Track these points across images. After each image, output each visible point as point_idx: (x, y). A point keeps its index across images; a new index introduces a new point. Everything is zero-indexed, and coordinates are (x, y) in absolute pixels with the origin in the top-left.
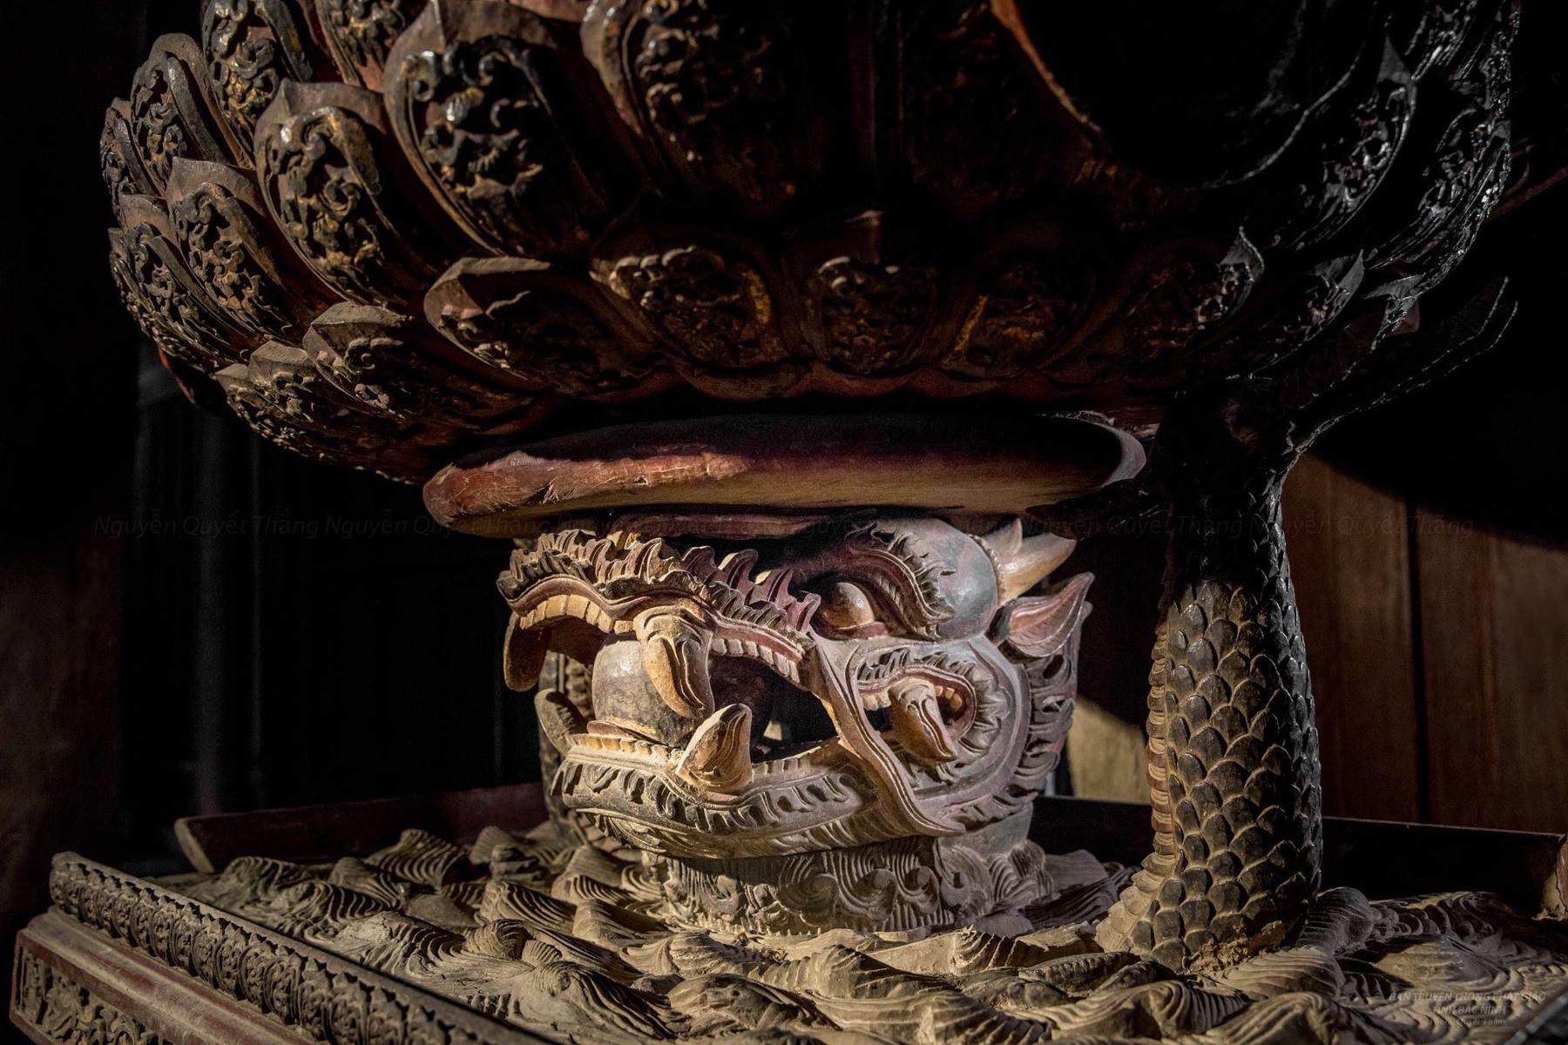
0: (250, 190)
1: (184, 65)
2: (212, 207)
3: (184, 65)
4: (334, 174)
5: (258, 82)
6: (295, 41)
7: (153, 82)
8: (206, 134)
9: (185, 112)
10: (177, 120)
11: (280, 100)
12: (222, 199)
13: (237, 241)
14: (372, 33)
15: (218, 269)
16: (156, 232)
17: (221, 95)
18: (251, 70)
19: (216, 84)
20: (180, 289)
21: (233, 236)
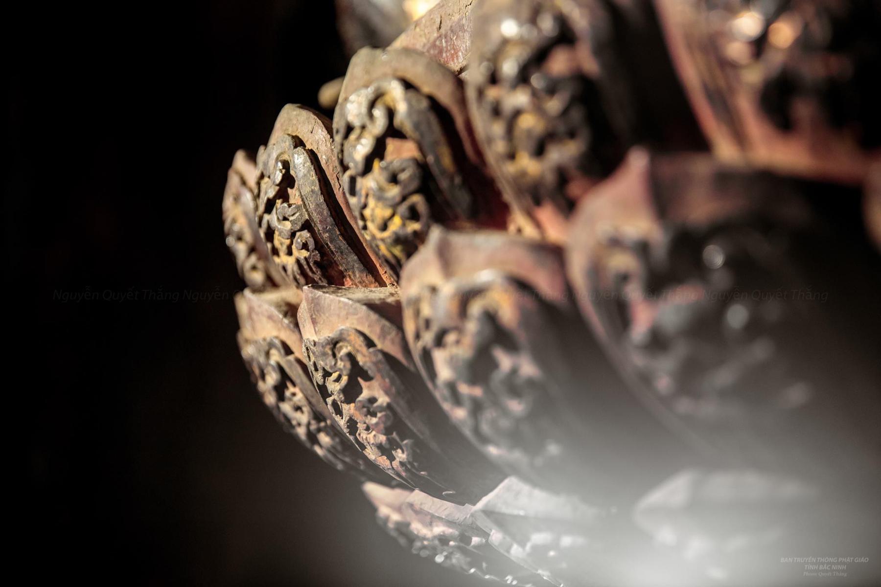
0: (398, 340)
1: (313, 157)
2: (351, 357)
3: (313, 157)
4: (505, 361)
5: (403, 208)
6: (447, 161)
7: (279, 177)
8: (343, 244)
9: (316, 217)
10: (307, 226)
11: (427, 253)
12: (364, 349)
13: (383, 400)
14: (550, 178)
15: (361, 426)
16: (288, 351)
17: (357, 214)
18: (394, 192)
19: (353, 201)
20: (318, 416)
21: (374, 390)
